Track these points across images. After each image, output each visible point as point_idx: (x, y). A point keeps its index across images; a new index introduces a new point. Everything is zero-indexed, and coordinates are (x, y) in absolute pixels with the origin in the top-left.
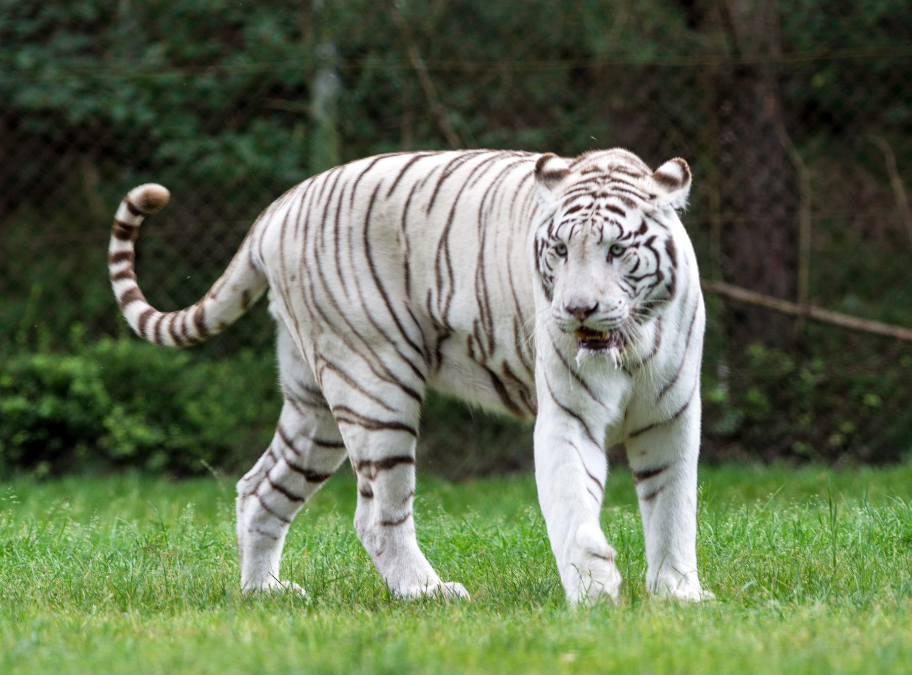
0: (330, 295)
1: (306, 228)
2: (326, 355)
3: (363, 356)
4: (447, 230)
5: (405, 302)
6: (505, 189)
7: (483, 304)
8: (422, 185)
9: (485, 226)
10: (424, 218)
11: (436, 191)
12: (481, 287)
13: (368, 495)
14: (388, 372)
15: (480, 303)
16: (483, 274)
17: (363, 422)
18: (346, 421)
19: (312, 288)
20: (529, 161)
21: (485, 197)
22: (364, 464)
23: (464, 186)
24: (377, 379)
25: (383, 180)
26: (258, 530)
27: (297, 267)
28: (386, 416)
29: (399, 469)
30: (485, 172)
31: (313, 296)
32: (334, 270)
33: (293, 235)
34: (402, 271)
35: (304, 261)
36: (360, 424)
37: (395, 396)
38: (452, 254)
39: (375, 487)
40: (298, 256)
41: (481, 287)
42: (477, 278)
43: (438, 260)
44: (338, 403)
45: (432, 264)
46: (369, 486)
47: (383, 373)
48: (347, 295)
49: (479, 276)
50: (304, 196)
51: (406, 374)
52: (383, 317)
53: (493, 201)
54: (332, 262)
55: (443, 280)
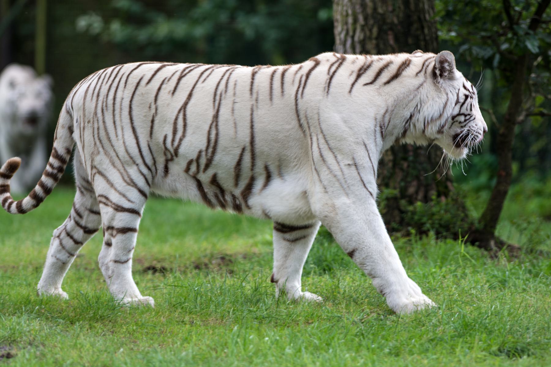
0: (107, 134)
1: (98, 95)
2: (98, 166)
3: (118, 170)
4: (186, 104)
5: (148, 141)
8: (169, 80)
10: (170, 97)
11: (178, 83)
12: (214, 132)
13: (109, 244)
14: (132, 180)
17: (113, 206)
18: (105, 204)
19: (98, 129)
22: (110, 228)
24: (125, 184)
25: (144, 75)
26: (56, 257)
27: (92, 116)
28: (127, 205)
29: (128, 234)
30: (210, 74)
31: (98, 133)
32: (112, 121)
33: (90, 98)
34: (150, 124)
35: (96, 113)
36: (112, 207)
37: (134, 194)
39: (114, 241)
40: (93, 110)
41: (214, 132)
43: (176, 119)
44: (101, 193)
45: (172, 121)
46: (111, 240)
47: (128, 180)
48: (117, 136)
50: (99, 78)
51: (141, 182)
52: (134, 151)
55: (178, 130)
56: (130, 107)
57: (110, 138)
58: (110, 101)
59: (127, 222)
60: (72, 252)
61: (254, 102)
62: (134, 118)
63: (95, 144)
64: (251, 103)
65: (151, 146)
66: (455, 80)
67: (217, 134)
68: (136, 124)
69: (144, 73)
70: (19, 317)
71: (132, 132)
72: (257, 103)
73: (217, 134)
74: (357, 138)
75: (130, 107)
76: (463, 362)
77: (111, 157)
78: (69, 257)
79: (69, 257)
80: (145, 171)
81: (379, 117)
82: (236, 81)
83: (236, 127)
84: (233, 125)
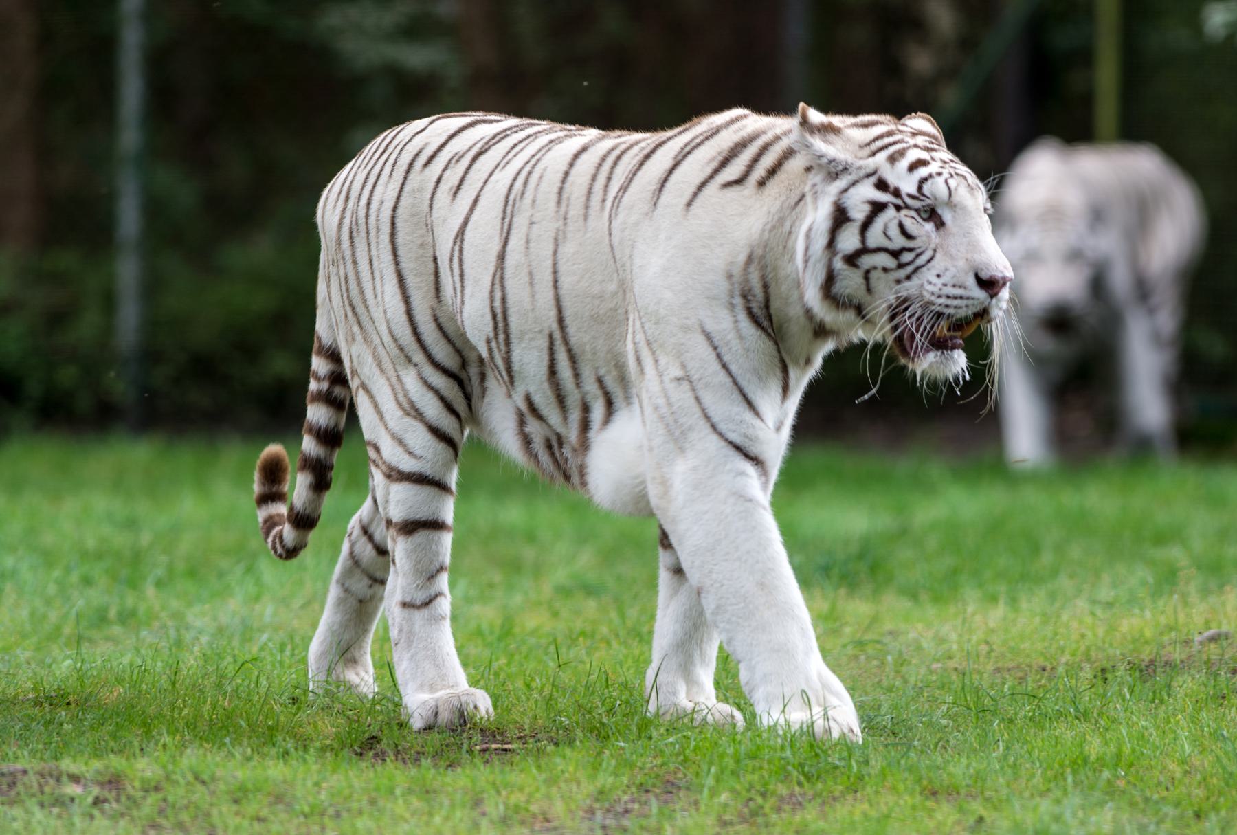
1: (347, 198)
5: (433, 309)
6: (545, 170)
7: (500, 317)
8: (458, 161)
9: (512, 216)
11: (468, 169)
14: (411, 403)
15: (494, 316)
16: (502, 278)
20: (579, 135)
21: (515, 179)
23: (496, 168)
29: (435, 535)
30: (524, 148)
38: (465, 253)
41: (498, 295)
42: (493, 284)
47: (406, 406)
49: (497, 281)
51: (432, 409)
53: (526, 183)
54: (365, 253)
56: (393, 224)
57: (366, 300)
58: (362, 212)
59: (411, 507)
60: (378, 575)
61: (561, 223)
62: (401, 252)
63: (346, 316)
64: (557, 225)
65: (441, 320)
66: (824, 179)
67: (504, 300)
68: (406, 265)
69: (428, 140)
70: (1058, 802)
71: (397, 285)
72: (565, 224)
73: (504, 300)
74: (687, 318)
75: (393, 224)
76: (515, 816)
77: (375, 348)
78: (371, 586)
79: (371, 586)
80: (438, 380)
81: (737, 271)
82: (547, 167)
83: (531, 284)
84: (527, 279)
